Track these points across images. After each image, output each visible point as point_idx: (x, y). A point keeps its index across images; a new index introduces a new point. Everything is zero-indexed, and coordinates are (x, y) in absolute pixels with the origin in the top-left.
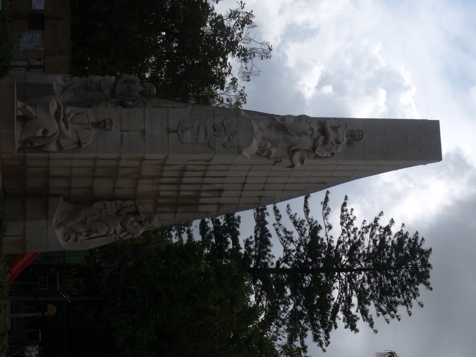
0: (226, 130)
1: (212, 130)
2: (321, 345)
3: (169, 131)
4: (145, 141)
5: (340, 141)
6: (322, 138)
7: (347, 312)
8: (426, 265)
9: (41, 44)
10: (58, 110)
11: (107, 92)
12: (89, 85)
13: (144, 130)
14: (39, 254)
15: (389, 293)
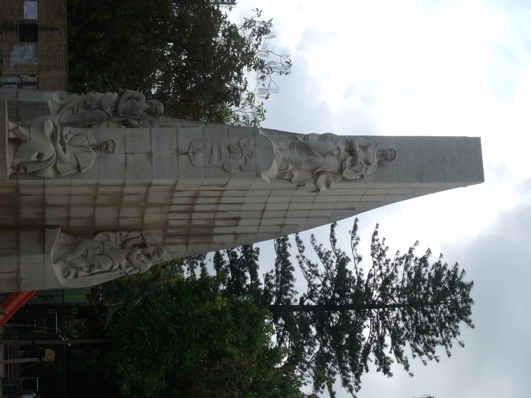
0: (242, 151)
1: (227, 151)
2: (351, 390)
3: (179, 153)
4: (152, 164)
5: (370, 161)
6: (350, 158)
7: (379, 354)
8: (467, 300)
11: (109, 110)
12: (88, 103)
13: (151, 153)
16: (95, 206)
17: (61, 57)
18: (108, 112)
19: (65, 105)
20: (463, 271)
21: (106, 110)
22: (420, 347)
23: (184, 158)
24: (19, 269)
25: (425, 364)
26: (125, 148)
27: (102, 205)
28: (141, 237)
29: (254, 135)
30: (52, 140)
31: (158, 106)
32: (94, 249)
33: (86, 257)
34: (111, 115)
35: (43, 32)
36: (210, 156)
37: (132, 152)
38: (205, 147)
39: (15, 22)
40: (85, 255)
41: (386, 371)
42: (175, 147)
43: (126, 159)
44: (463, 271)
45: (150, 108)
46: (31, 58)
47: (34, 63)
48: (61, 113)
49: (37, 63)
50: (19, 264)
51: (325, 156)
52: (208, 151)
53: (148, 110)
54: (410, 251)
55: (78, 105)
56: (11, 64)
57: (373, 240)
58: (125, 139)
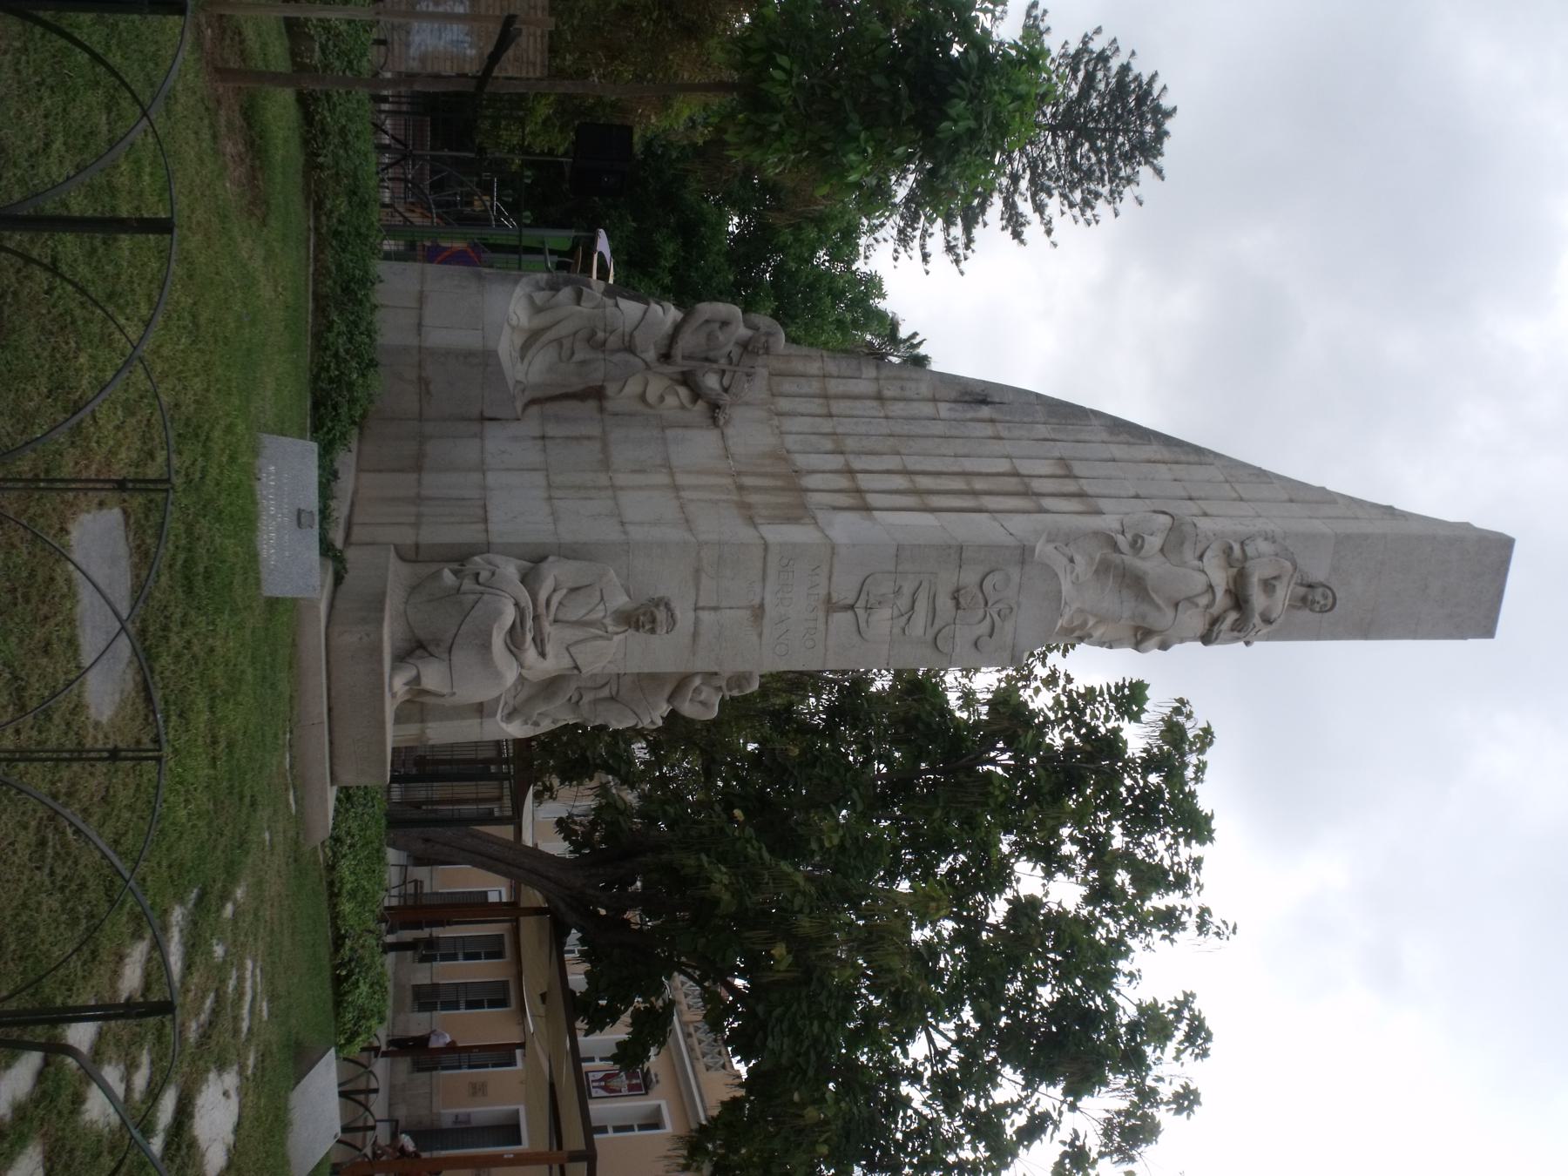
0: (986, 604)
1: (950, 604)
2: (957, 262)
3: (830, 606)
4: (760, 635)
5: (1274, 616)
6: (1233, 616)
7: (1010, 206)
8: (1161, 135)
9: (468, 39)
10: (518, 621)
11: (651, 355)
12: (601, 335)
13: (762, 606)
14: (446, 254)
15: (1088, 175)
17: (531, 39)
18: (648, 360)
20: (1165, 88)
21: (643, 356)
22: (1077, 196)
23: (842, 619)
25: (1076, 222)
26: (697, 595)
29: (1023, 563)
30: (512, 640)
31: (771, 340)
32: (595, 689)
33: (578, 702)
36: (906, 616)
37: (713, 604)
38: (898, 592)
40: (574, 700)
41: (1017, 235)
42: (823, 592)
43: (697, 621)
44: (1165, 88)
45: (750, 338)
46: (461, 37)
47: (468, 52)
49: (474, 52)
51: (1176, 605)
52: (904, 603)
54: (1085, 43)
55: (575, 334)
56: (413, 52)
57: (1028, 15)
58: (697, 572)
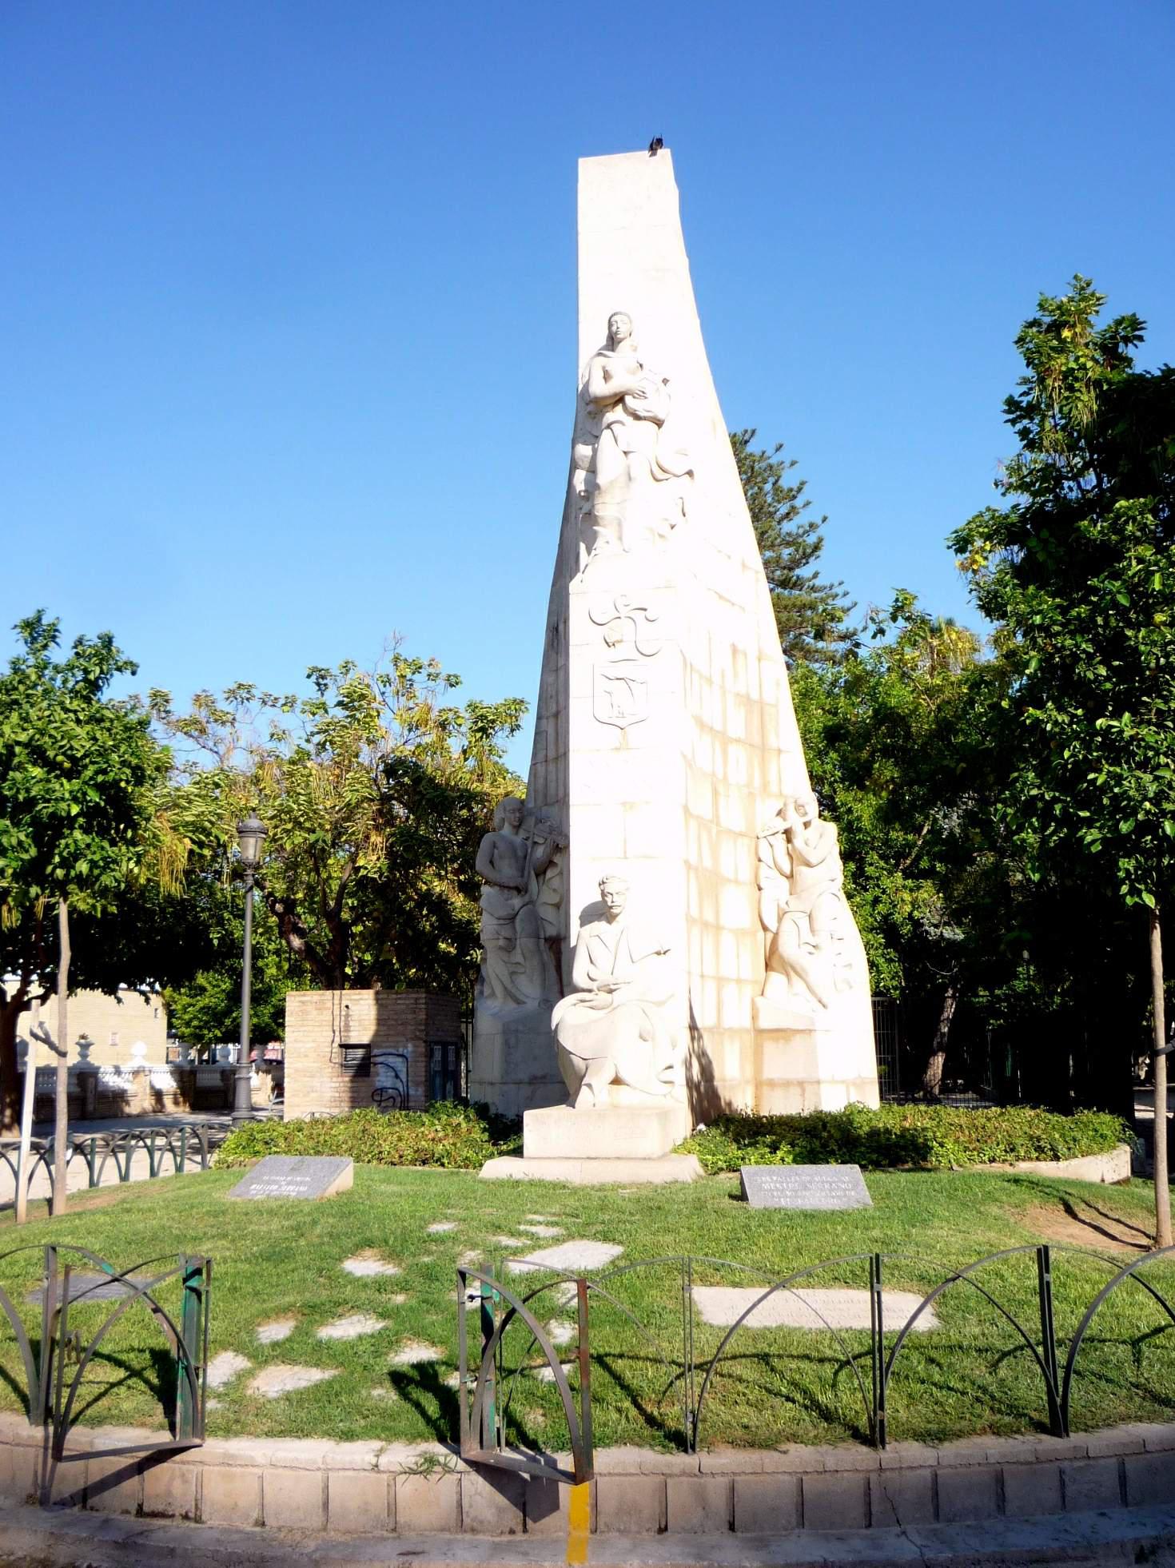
11: (517, 902)
16: (718, 928)
19: (505, 989)
21: (517, 908)
24: (843, 1082)
27: (717, 913)
28: (771, 839)
34: (527, 898)
35: (352, 1034)
39: (333, 1085)
48: (521, 998)
50: (834, 1081)
53: (514, 827)
